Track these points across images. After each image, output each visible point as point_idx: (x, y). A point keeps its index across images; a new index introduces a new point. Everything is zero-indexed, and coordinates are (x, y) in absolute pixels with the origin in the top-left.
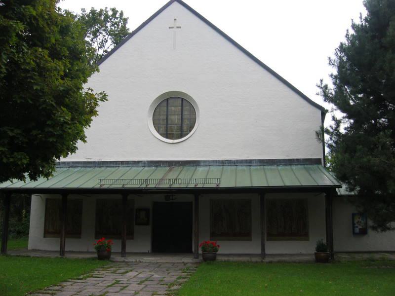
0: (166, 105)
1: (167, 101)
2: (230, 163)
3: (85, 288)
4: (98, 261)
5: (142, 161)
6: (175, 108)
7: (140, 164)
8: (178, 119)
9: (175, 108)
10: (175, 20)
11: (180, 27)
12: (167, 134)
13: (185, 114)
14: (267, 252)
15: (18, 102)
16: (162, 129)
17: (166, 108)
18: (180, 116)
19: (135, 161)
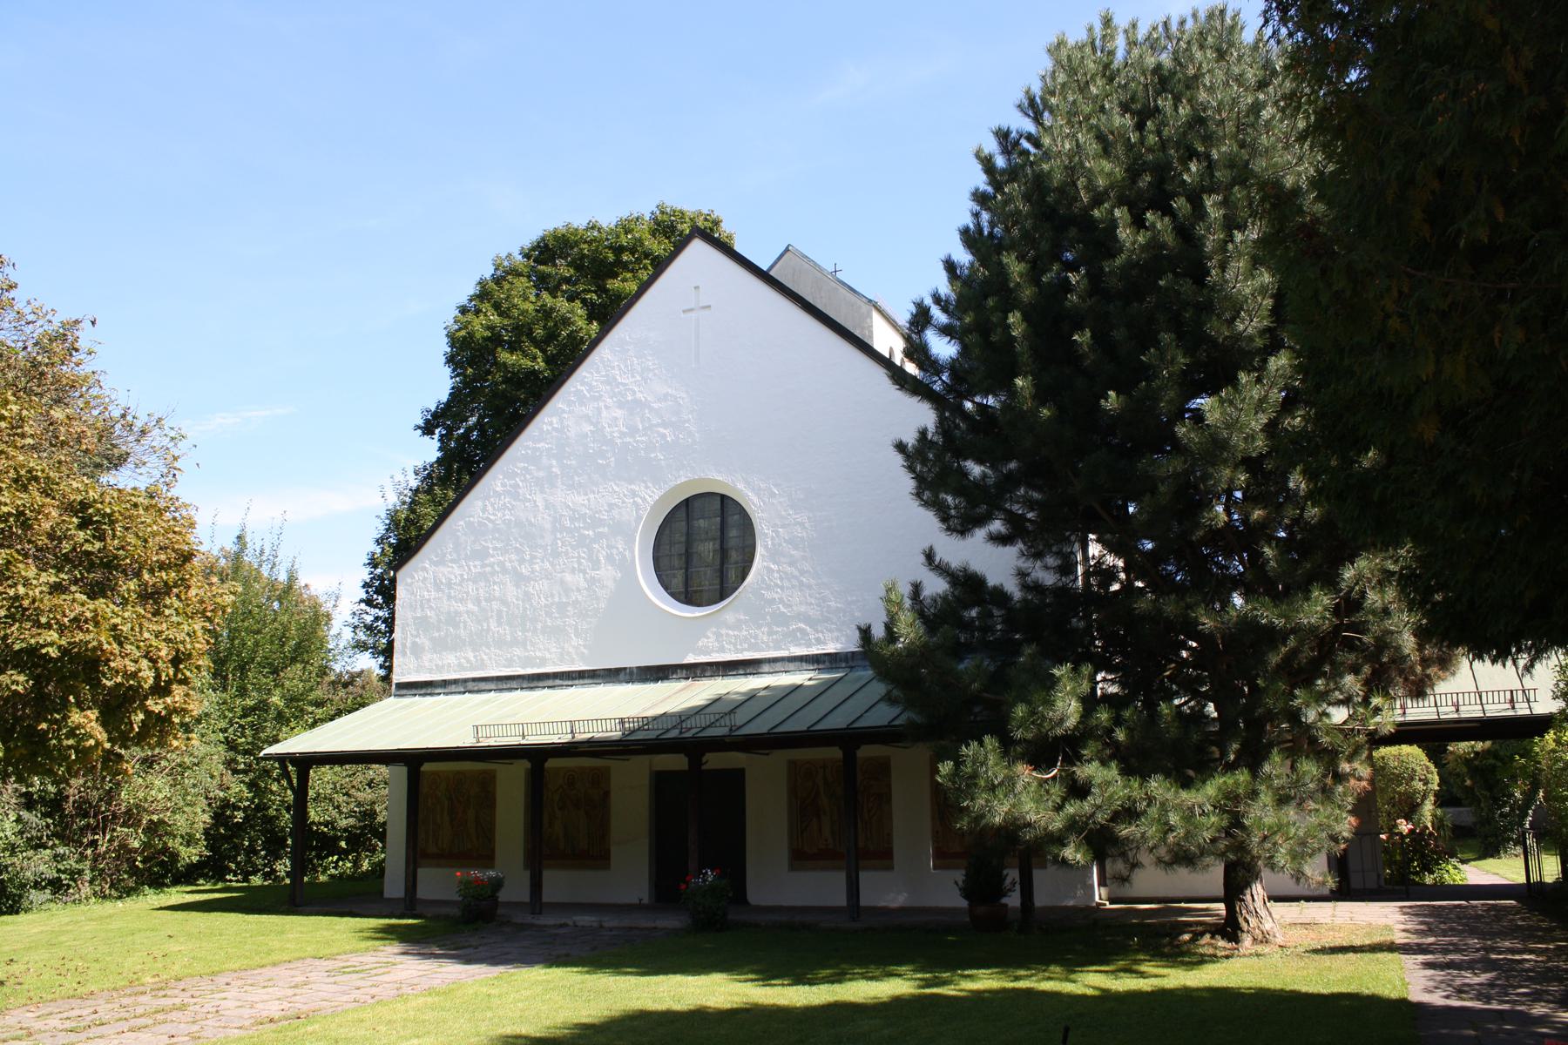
0: (684, 515)
1: (687, 505)
2: (836, 661)
3: (434, 976)
4: (52, 905)
5: (625, 669)
6: (706, 524)
7: (622, 676)
8: (714, 551)
9: (706, 524)
10: (697, 288)
11: (709, 307)
12: (687, 592)
13: (731, 535)
14: (548, 896)
15: (1440, 119)
16: (678, 581)
17: (684, 523)
18: (718, 542)
19: (610, 670)
